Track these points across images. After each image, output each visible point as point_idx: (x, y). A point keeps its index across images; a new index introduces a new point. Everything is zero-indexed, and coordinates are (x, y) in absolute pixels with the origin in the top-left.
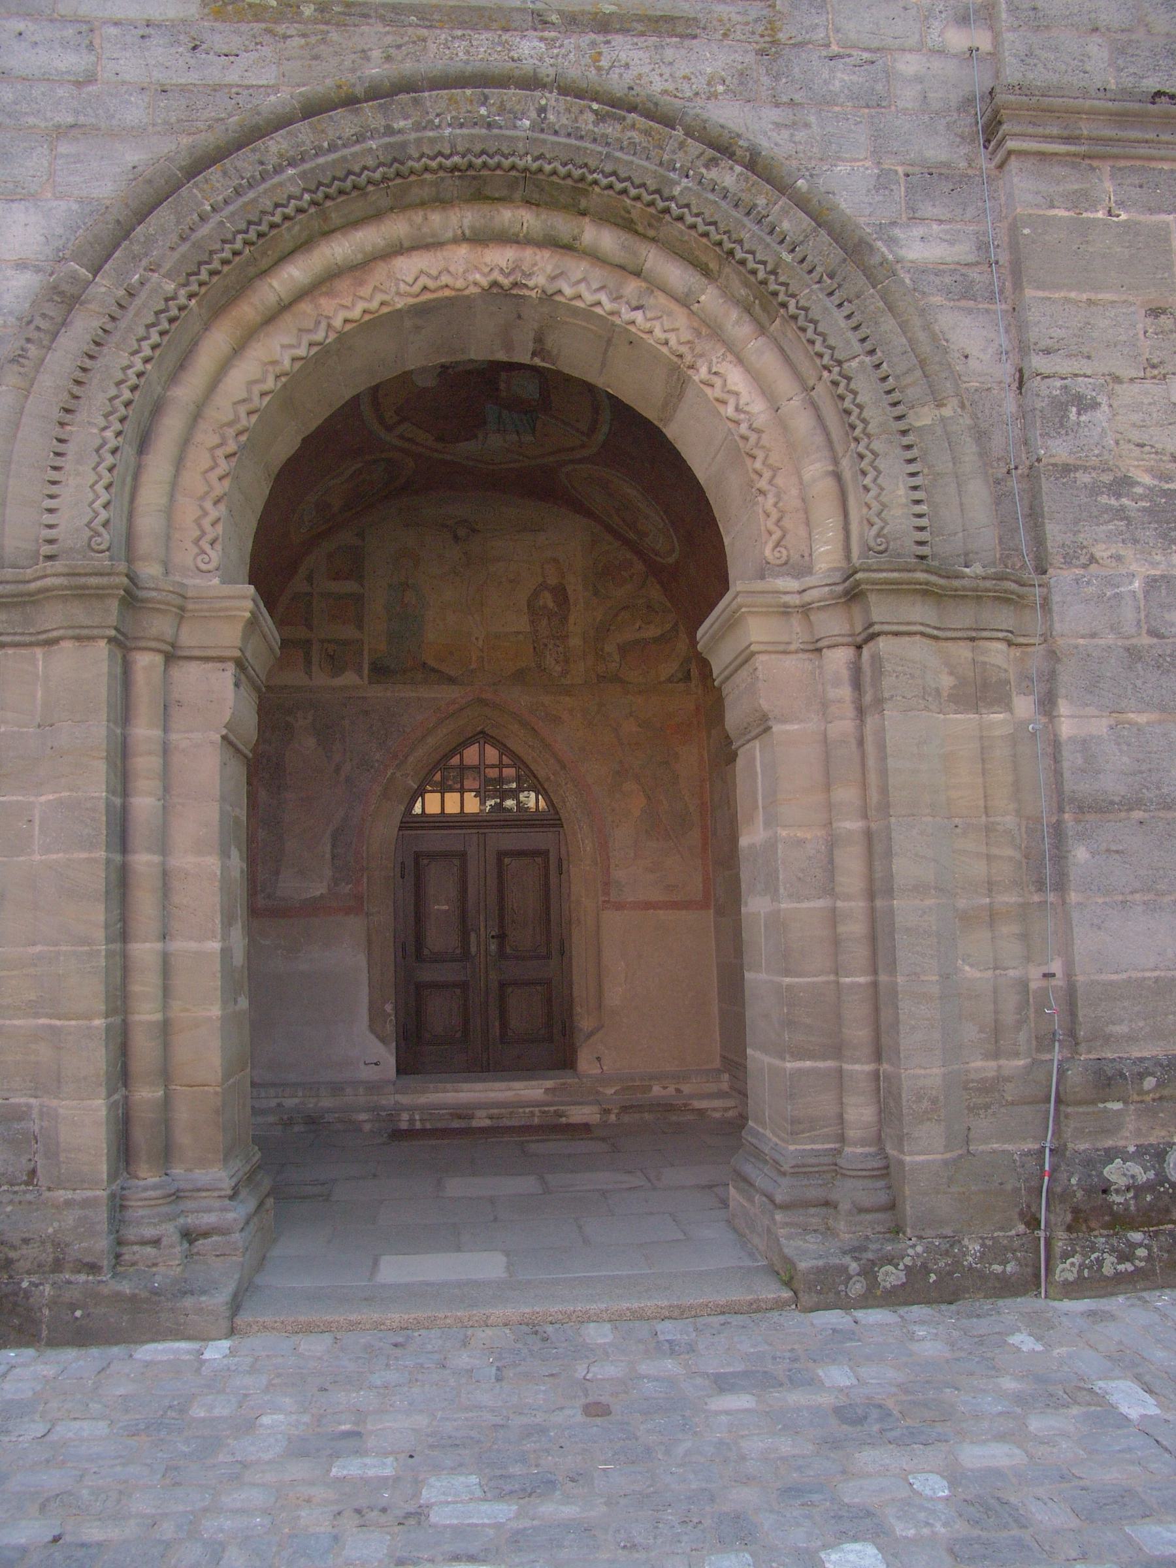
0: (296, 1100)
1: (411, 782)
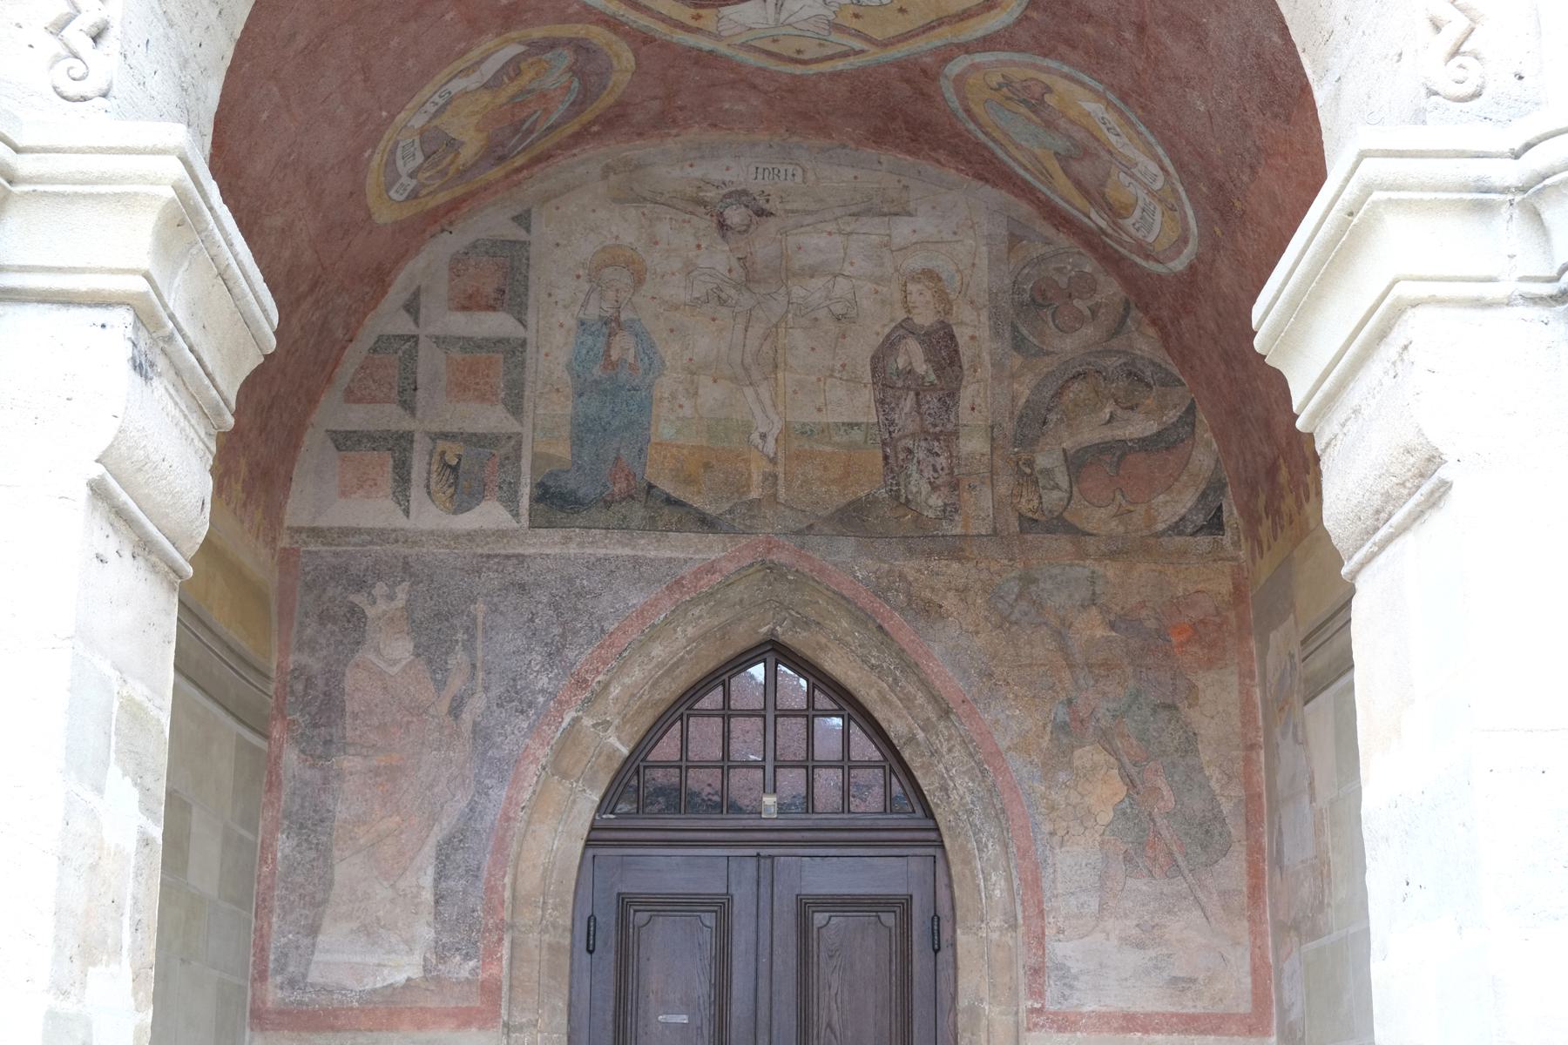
1: (613, 741)
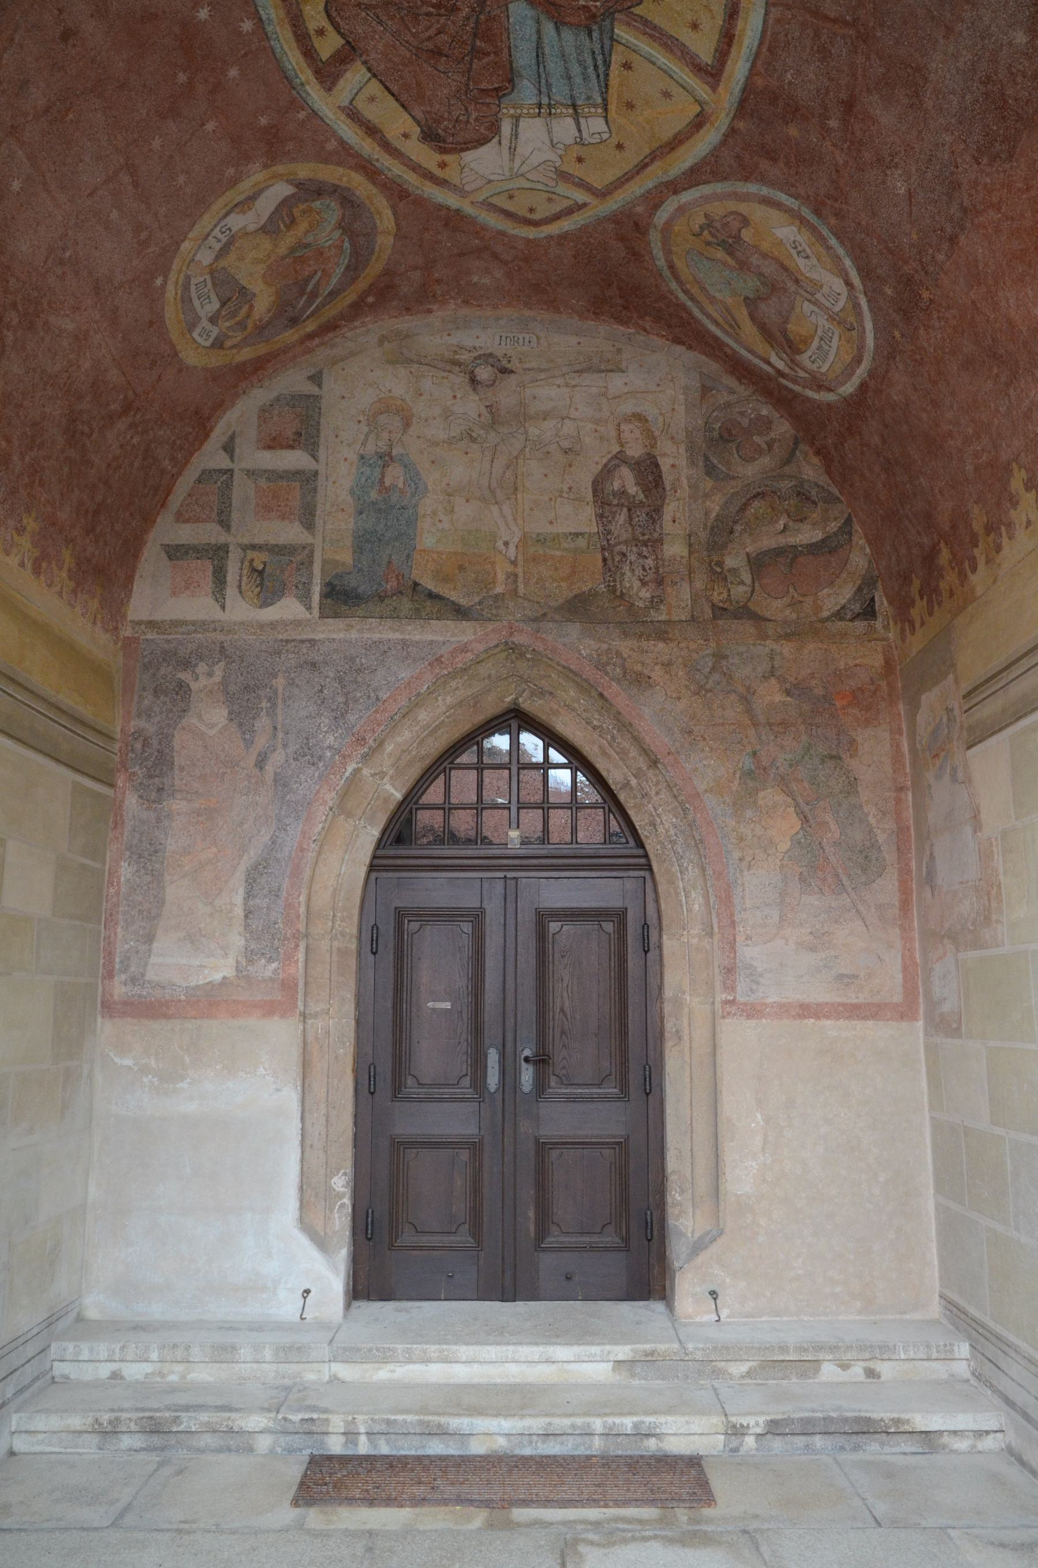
0: (148, 1368)
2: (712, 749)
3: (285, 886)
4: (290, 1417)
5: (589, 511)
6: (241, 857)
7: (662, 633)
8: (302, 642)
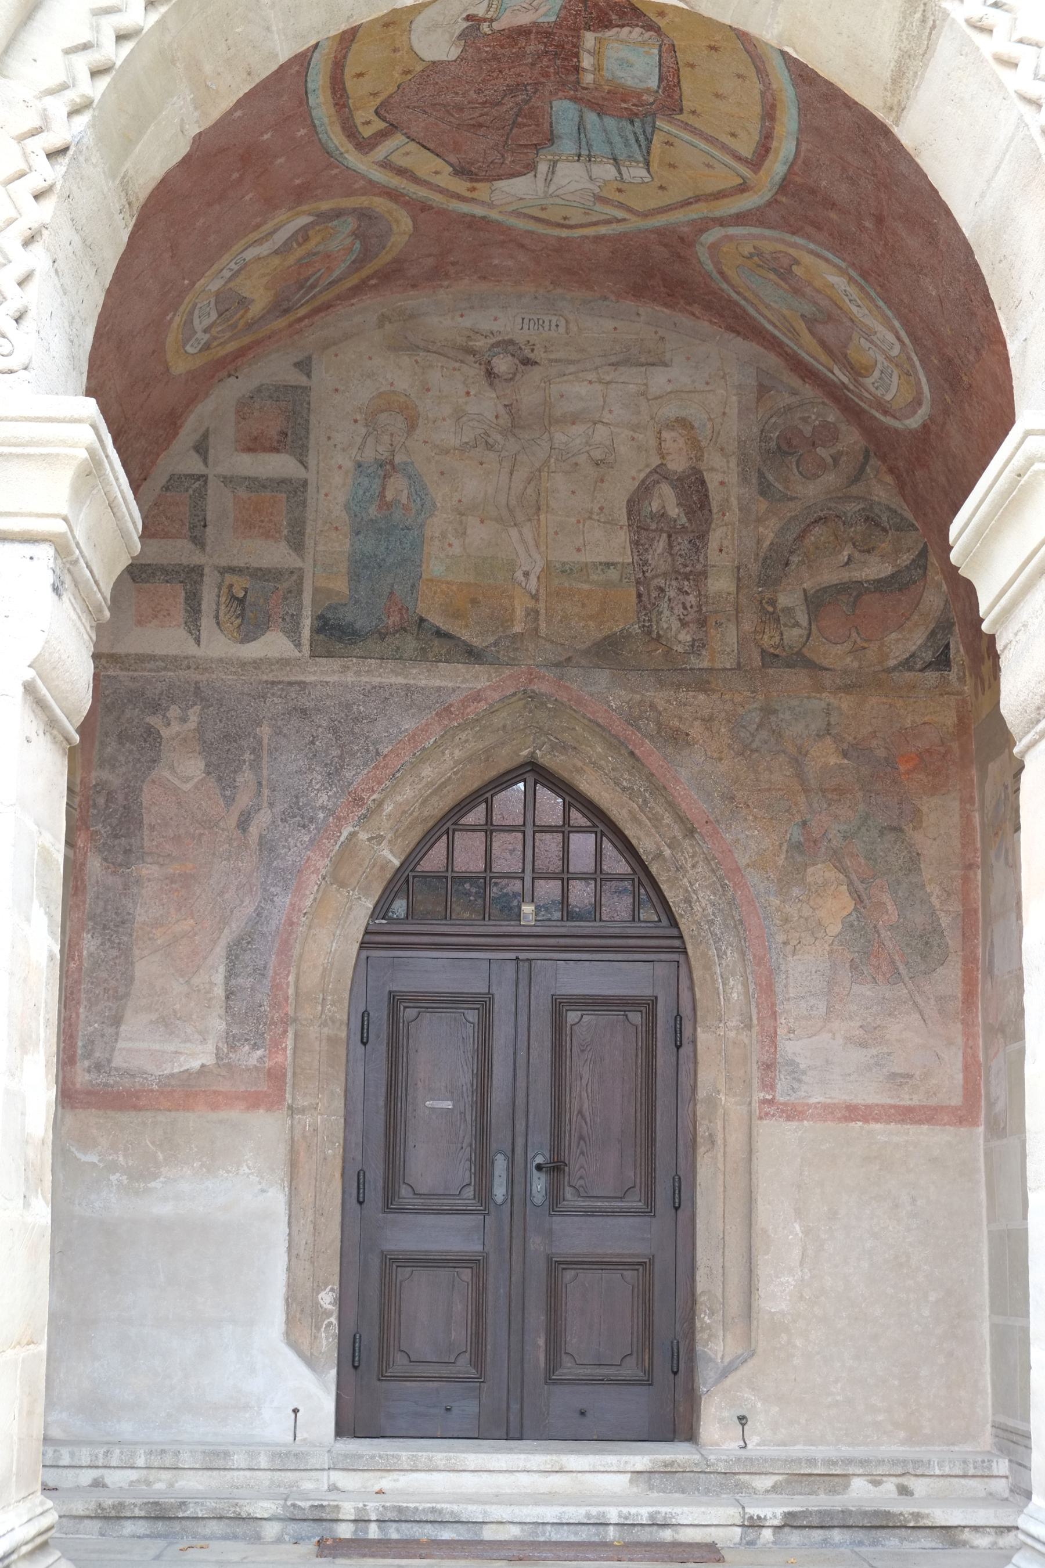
1: (387, 853)
2: (756, 818)
3: (271, 966)
4: (299, 1503)
5: (622, 537)
6: (221, 930)
7: (702, 682)
8: (290, 684)
